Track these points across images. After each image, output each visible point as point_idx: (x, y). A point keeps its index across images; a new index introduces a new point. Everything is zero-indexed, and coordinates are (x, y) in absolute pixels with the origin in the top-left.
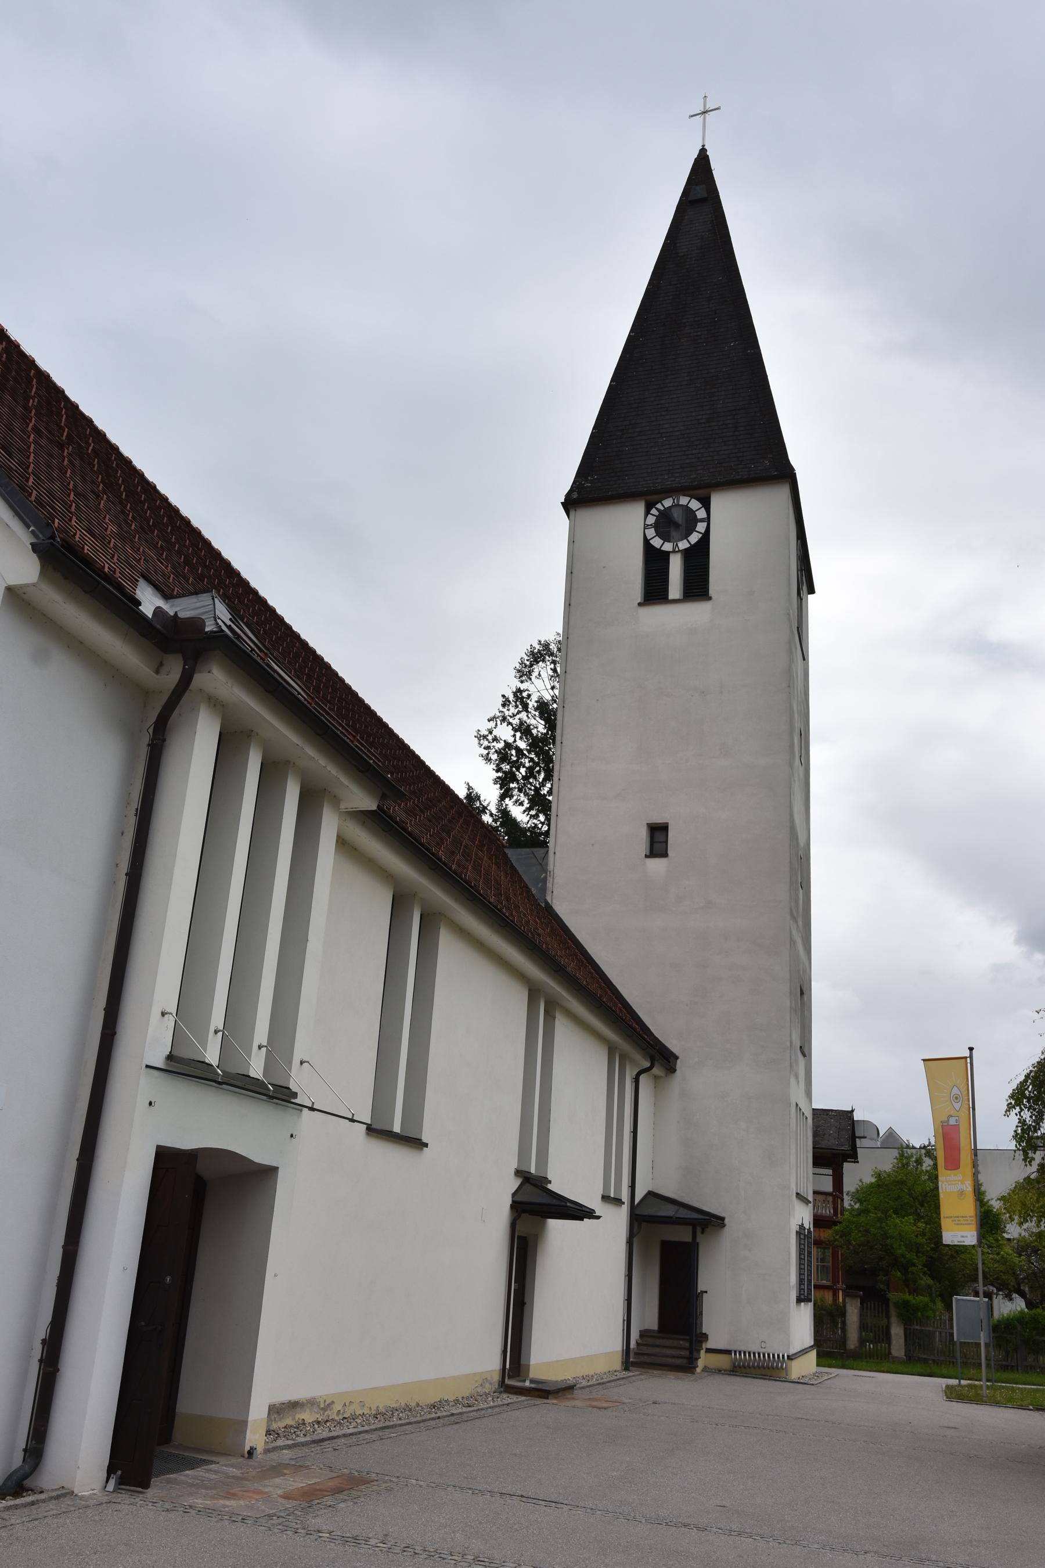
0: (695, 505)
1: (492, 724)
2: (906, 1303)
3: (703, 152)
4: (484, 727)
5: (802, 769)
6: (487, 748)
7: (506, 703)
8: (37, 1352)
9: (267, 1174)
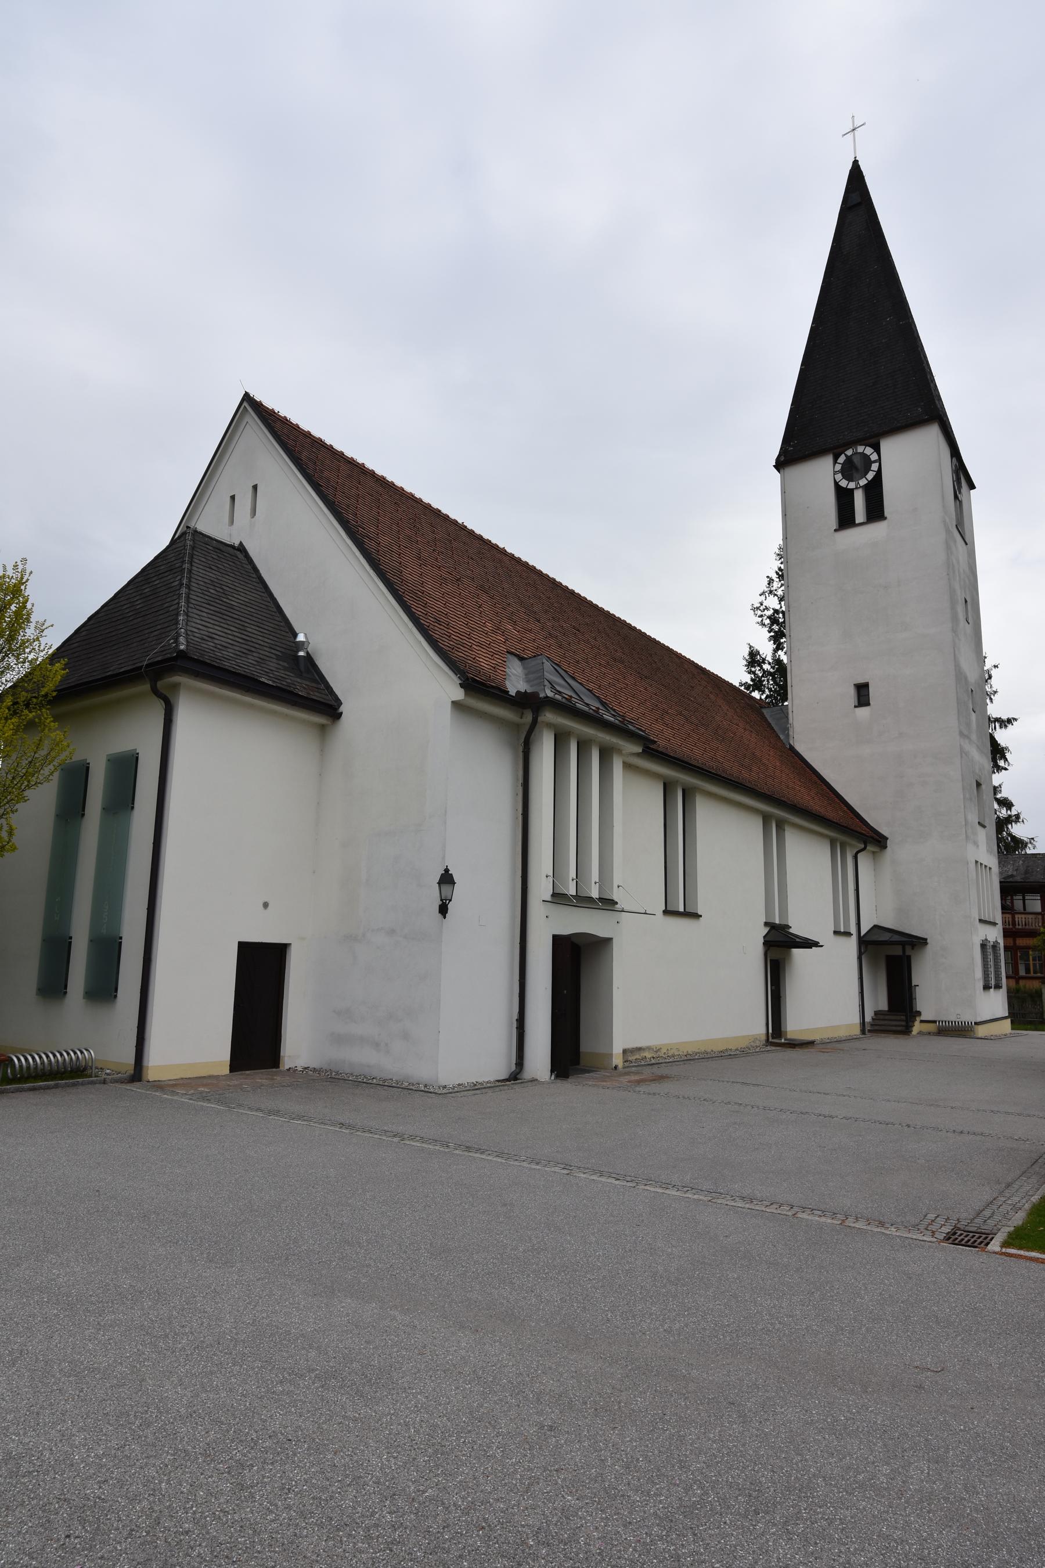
0: (869, 451)
1: (763, 597)
3: (856, 165)
5: (969, 628)
6: (761, 616)
7: (771, 581)
8: (515, 1025)
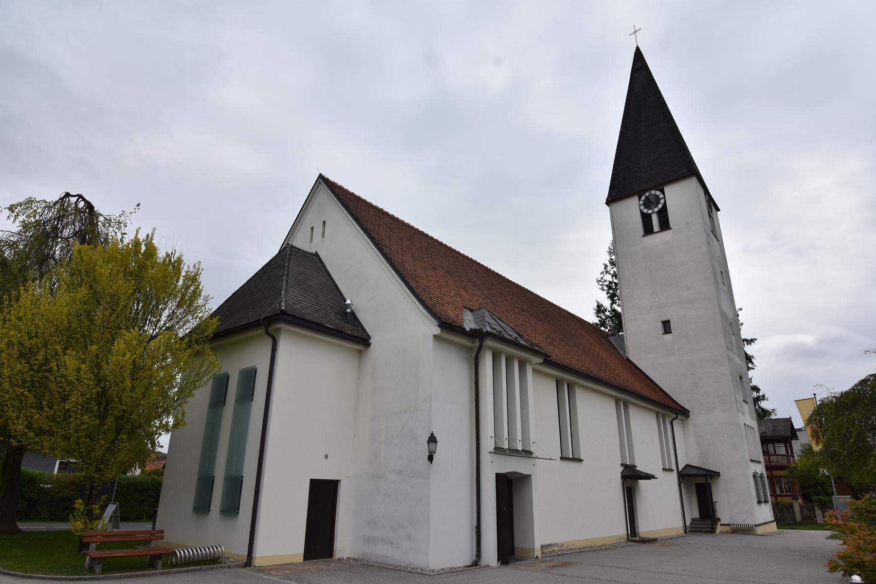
0: (658, 193)
2: (821, 500)
4: (599, 277)
5: (725, 288)
7: (606, 266)
9: (528, 477)
